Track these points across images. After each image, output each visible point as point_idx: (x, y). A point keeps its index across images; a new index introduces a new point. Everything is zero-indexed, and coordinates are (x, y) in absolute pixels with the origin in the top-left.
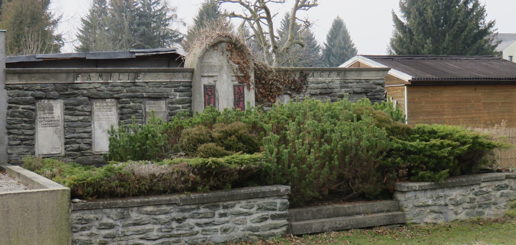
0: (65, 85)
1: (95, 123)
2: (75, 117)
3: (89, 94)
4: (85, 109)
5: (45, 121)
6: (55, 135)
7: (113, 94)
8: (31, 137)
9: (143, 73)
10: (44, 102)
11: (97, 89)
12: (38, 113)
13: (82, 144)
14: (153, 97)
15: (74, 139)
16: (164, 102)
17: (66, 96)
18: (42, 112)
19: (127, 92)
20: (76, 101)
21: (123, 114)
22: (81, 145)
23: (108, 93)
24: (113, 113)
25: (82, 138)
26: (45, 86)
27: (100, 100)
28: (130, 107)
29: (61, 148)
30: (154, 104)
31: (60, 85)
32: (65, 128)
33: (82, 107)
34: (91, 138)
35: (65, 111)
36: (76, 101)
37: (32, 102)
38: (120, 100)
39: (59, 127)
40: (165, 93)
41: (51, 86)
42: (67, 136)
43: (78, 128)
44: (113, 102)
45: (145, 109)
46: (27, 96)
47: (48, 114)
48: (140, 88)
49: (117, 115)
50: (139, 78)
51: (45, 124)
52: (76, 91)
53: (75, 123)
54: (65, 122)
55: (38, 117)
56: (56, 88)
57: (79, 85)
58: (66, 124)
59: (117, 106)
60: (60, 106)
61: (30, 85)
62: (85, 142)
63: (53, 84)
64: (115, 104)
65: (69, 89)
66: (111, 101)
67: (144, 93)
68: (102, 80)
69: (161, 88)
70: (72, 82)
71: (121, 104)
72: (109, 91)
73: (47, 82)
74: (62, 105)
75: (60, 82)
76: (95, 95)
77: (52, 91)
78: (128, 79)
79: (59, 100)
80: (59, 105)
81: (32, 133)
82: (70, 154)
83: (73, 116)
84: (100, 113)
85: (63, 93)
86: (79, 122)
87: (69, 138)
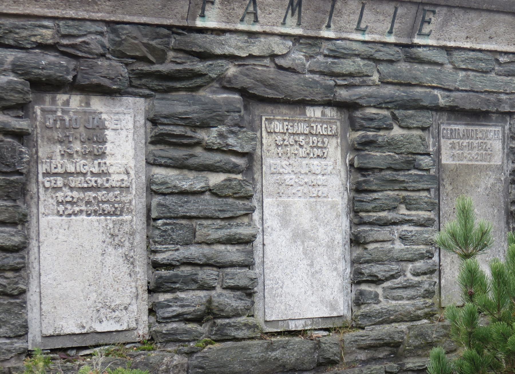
0: (158, 36)
1: (267, 201)
2: (191, 175)
3: (247, 82)
4: (231, 141)
5: (71, 189)
6: (110, 249)
7: (336, 85)
8: (12, 259)
9: (445, 10)
10: (67, 103)
11: (277, 61)
12: (43, 152)
13: (219, 290)
14: (468, 107)
15: (187, 270)
16: (499, 129)
17: (154, 84)
18: (58, 148)
19: (384, 83)
20: (197, 107)
21: (367, 169)
22: (213, 293)
23: (316, 82)
24: (329, 162)
25: (221, 266)
26: (75, 32)
27: (284, 110)
28: (391, 144)
29: (134, 307)
30: (467, 136)
31: (134, 31)
32: (149, 219)
33: (221, 135)
34: (249, 265)
35: (152, 147)
36: (197, 107)
37: (16, 98)
38: (358, 114)
39: (126, 217)
40: (503, 97)
41: (101, 34)
42: (160, 257)
43: (205, 222)
44: (329, 122)
45: (439, 152)
46: (150, 205)
47: (84, 155)
48: (425, 72)
49: (343, 174)
50: (426, 29)
51: (71, 203)
52: (200, 66)
53: (192, 198)
54: (151, 192)
55: (42, 169)
56: (120, 43)
57: (210, 37)
58: (159, 205)
59: (344, 137)
60: (131, 126)
61: (12, 21)
62: (231, 283)
63: (108, 23)
64: (336, 127)
65: (171, 54)
66: (323, 114)
67: (436, 92)
68: (299, 24)
69: (493, 75)
70: (185, 23)
71: (363, 128)
72: (322, 73)
73: (82, 14)
74: (141, 120)
75: (136, 20)
76: (271, 86)
77: (103, 55)
78: (390, 32)
79: (130, 100)
80: (128, 121)
81: (17, 239)
82: (175, 332)
83: (186, 172)
84: (284, 163)
85: (146, 68)
86: (207, 196)
87: (169, 266)
